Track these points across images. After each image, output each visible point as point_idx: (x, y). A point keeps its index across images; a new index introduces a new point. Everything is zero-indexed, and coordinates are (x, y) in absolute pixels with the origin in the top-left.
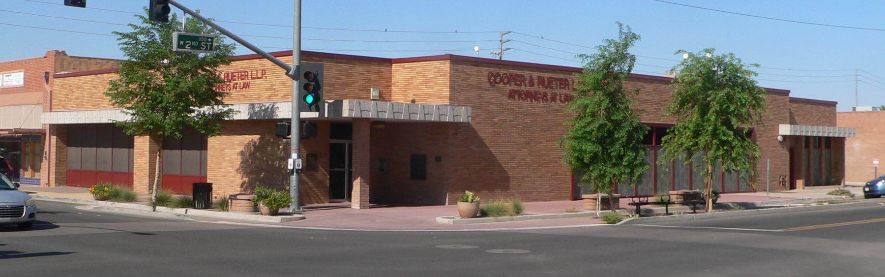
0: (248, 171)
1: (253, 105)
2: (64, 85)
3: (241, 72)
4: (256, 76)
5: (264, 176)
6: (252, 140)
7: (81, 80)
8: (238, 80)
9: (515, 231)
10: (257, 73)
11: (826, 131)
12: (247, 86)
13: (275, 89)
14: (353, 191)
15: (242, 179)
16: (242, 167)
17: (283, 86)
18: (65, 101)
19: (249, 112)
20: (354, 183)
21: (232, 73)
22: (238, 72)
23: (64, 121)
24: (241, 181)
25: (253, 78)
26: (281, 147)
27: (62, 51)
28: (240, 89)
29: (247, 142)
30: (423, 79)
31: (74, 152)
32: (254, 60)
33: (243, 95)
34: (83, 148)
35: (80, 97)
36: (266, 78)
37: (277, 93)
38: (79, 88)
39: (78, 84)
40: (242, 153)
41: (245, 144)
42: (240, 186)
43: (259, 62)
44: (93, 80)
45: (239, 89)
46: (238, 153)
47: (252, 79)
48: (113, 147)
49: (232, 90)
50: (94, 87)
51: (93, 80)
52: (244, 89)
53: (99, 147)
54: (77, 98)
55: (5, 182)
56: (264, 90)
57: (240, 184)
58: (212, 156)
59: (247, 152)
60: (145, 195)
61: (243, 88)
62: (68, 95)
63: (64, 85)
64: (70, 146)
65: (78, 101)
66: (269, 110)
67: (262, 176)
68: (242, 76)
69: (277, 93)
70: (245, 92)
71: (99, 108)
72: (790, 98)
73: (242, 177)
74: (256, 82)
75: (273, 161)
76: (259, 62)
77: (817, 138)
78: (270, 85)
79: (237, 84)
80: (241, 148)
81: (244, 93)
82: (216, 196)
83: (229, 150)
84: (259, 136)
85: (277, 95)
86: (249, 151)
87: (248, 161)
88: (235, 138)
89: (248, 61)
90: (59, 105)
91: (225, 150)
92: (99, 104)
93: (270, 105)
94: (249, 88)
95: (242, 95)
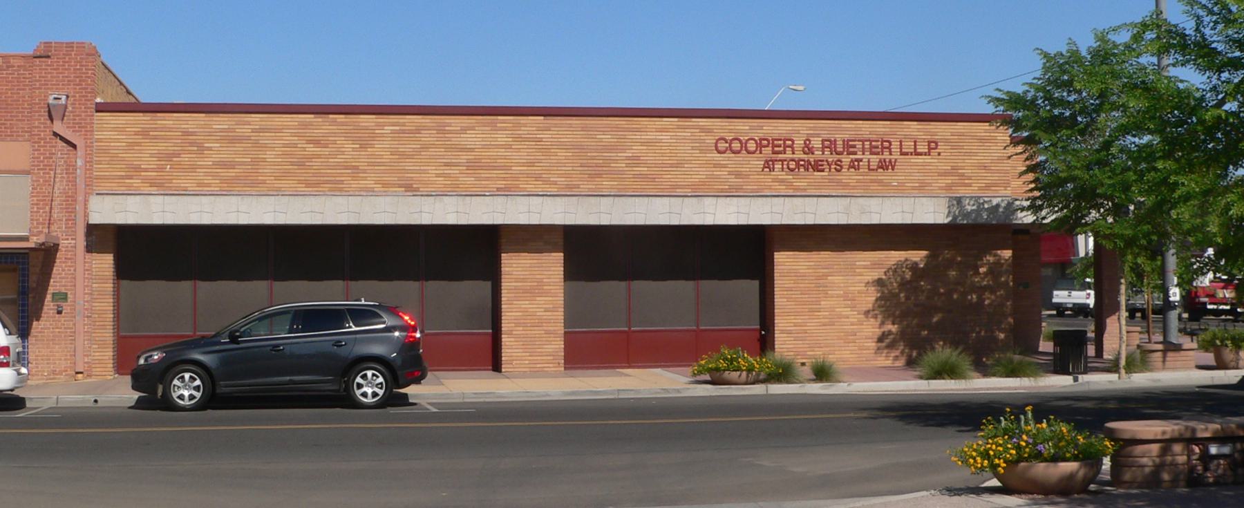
0: (897, 313)
1: (959, 200)
2: (155, 129)
3: (871, 141)
6: (906, 260)
10: (901, 145)
13: (963, 175)
14: (1107, 331)
15: (880, 328)
16: (879, 307)
19: (949, 212)
20: (1108, 321)
22: (863, 141)
23: (529, 220)
24: (878, 332)
26: (982, 270)
27: (1058, 52)
29: (893, 263)
30: (311, 164)
31: (156, 291)
33: (880, 182)
40: (879, 283)
41: (889, 266)
42: (876, 340)
43: (375, 120)
46: (868, 283)
47: (901, 154)
55: (1238, 390)
57: (876, 337)
59: (892, 280)
63: (155, 129)
66: (1001, 210)
67: (935, 320)
68: (872, 147)
70: (882, 175)
73: (882, 323)
75: (964, 294)
76: (375, 120)
77: (89, 239)
78: (949, 168)
79: (860, 160)
80: (878, 274)
82: (804, 361)
84: (924, 253)
86: (899, 279)
87: (897, 295)
88: (858, 256)
89: (889, 123)
90: (131, 177)
93: (1002, 201)
94: (893, 169)
95: (872, 181)
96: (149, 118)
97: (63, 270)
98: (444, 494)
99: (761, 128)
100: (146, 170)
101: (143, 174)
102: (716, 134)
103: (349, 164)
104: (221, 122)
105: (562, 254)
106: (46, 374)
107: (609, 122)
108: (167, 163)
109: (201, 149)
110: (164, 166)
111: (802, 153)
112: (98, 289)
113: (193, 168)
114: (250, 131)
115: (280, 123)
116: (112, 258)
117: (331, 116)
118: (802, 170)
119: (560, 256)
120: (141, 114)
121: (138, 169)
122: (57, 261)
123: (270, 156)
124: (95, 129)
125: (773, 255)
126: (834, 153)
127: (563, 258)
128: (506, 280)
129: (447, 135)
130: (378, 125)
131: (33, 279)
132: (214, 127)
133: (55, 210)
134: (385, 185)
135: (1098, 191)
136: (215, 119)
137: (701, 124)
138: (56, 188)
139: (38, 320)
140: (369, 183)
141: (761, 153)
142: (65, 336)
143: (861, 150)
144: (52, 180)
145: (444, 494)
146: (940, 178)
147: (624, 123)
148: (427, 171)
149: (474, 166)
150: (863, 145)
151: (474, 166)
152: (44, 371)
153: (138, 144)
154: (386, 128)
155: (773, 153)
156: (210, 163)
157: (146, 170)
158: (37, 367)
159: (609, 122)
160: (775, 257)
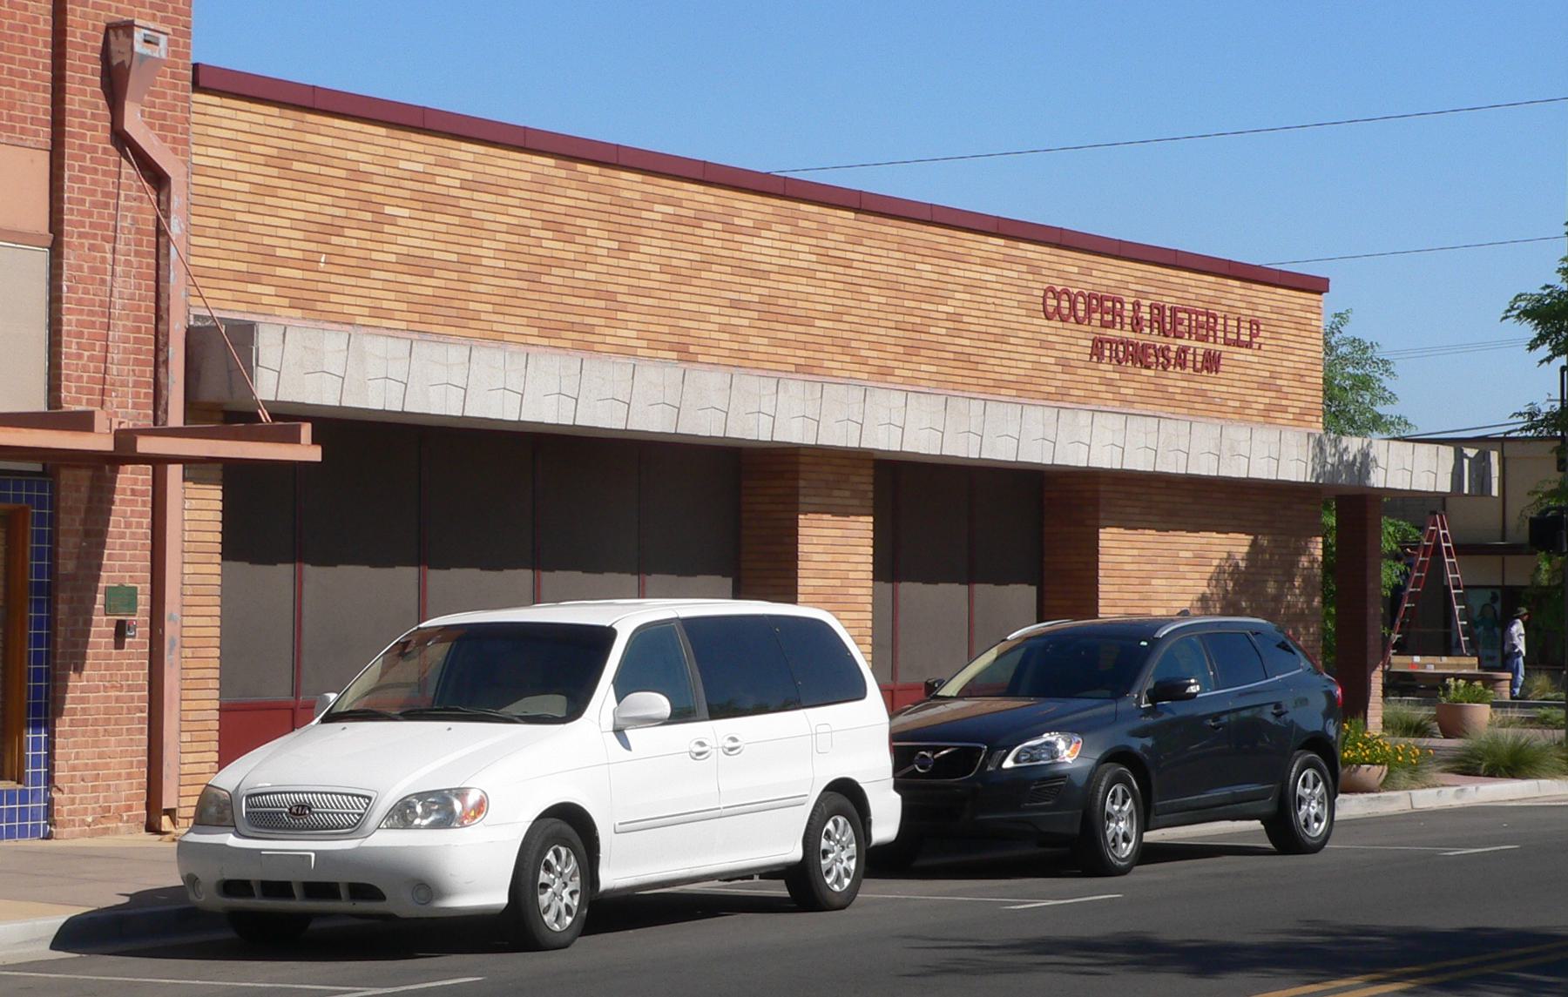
2: (302, 156)
4: (1235, 337)
5: (1144, 646)
7: (454, 164)
8: (1189, 339)
9: (946, 719)
11: (334, 363)
12: (1212, 362)
17: (1297, 384)
18: (308, 263)
21: (1174, 311)
25: (1227, 343)
28: (1195, 369)
32: (1230, 282)
33: (1202, 393)
34: (309, 570)
35: (445, 266)
36: (1260, 348)
37: (1284, 402)
38: (431, 203)
39: (426, 178)
43: (1242, 291)
44: (542, 184)
45: (1191, 371)
48: (970, 578)
49: (1171, 368)
50: (548, 225)
51: (542, 184)
52: (1205, 372)
53: (551, 568)
54: (419, 265)
56: (1255, 386)
58: (823, 574)
60: (1383, 771)
61: (1202, 370)
62: (338, 231)
63: (302, 156)
64: (313, 564)
65: (426, 287)
69: (1284, 402)
70: (1206, 381)
71: (589, 348)
72: (1489, 453)
74: (1236, 357)
81: (1205, 387)
83: (1164, 582)
85: (1284, 410)
89: (1212, 279)
90: (254, 278)
91: (1154, 582)
92: (590, 329)
96: (289, 124)
97: (128, 525)
98: (1270, 799)
99: (1087, 272)
100: (285, 262)
101: (280, 271)
102: (1046, 279)
103: (603, 287)
104: (415, 152)
105: (871, 519)
106: (90, 819)
107: (928, 236)
108: (321, 248)
109: (381, 220)
110: (315, 257)
111: (1043, 315)
112: (198, 579)
113: (366, 266)
114: (457, 183)
115: (504, 172)
116: (219, 495)
117: (581, 167)
118: (1160, 368)
119: (863, 526)
120: (275, 111)
121: (270, 257)
122: (117, 497)
123: (487, 251)
124: (193, 138)
125: (1097, 533)
126: (1162, 334)
127: (871, 527)
128: (807, 573)
129: (737, 238)
130: (649, 199)
131: (68, 545)
132: (402, 164)
133: (115, 356)
134: (654, 343)
135: (107, 467)
136: (404, 145)
137: (1029, 255)
138: (116, 294)
139: (79, 669)
140: (627, 335)
141: (1089, 324)
142: (129, 711)
143: (1149, 325)
144: (109, 268)
145: (1270, 799)
146: (1261, 393)
147: (945, 240)
148: (1052, 346)
149: (770, 312)
150: (1190, 317)
151: (770, 312)
152: (85, 811)
153: (271, 190)
154: (657, 207)
155: (1102, 326)
156: (393, 258)
157: (285, 262)
158: (73, 802)
159: (928, 236)
160: (1101, 536)
